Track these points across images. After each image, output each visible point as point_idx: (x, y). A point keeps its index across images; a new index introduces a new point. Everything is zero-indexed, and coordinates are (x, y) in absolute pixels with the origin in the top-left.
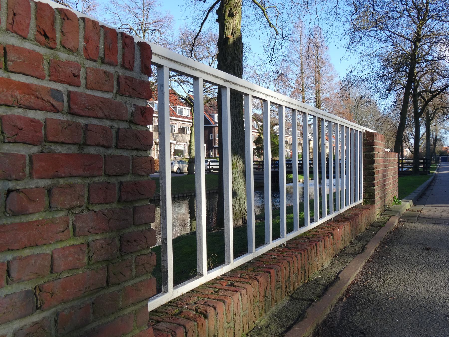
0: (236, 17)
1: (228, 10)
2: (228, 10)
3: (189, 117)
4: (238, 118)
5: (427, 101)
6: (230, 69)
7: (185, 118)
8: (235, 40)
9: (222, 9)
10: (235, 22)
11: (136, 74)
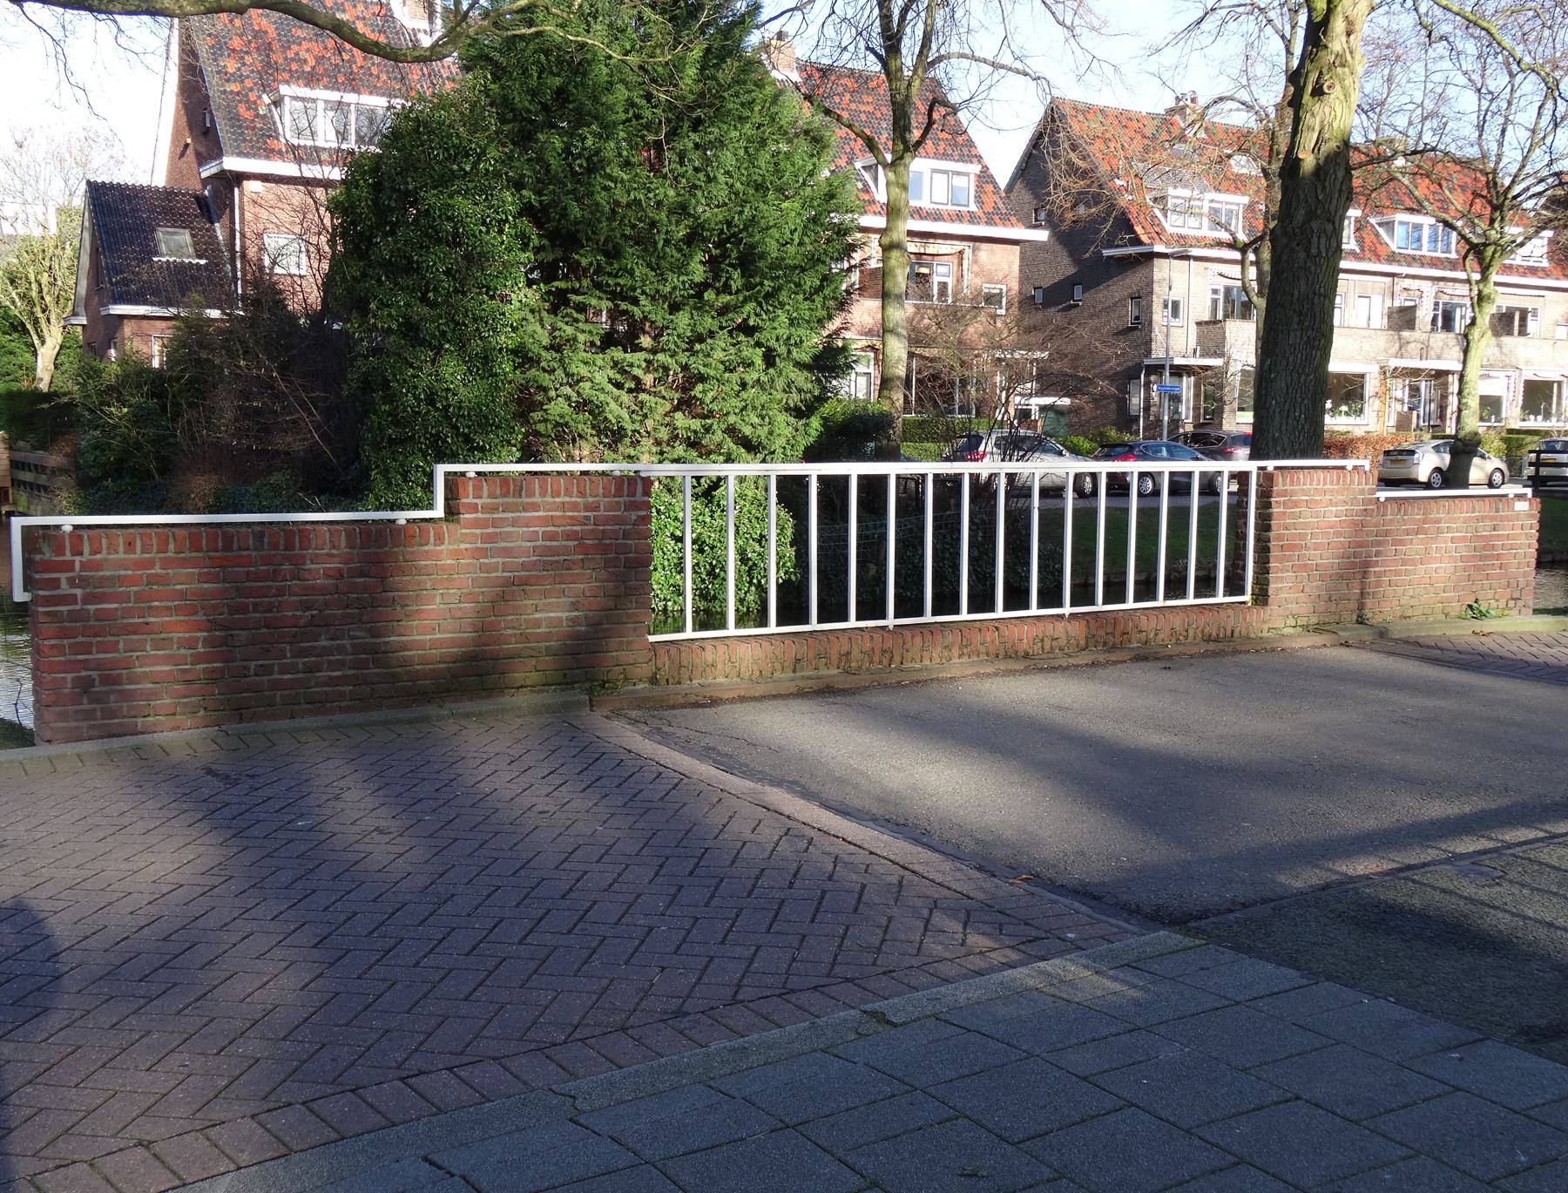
0: (1332, 96)
1: (1313, 77)
2: (1313, 77)
3: (1543, 269)
4: (1303, 378)
5: (1245, 444)
6: (1298, 245)
7: (1524, 275)
8: (1321, 162)
9: (1300, 76)
10: (1327, 110)
11: (639, 497)
